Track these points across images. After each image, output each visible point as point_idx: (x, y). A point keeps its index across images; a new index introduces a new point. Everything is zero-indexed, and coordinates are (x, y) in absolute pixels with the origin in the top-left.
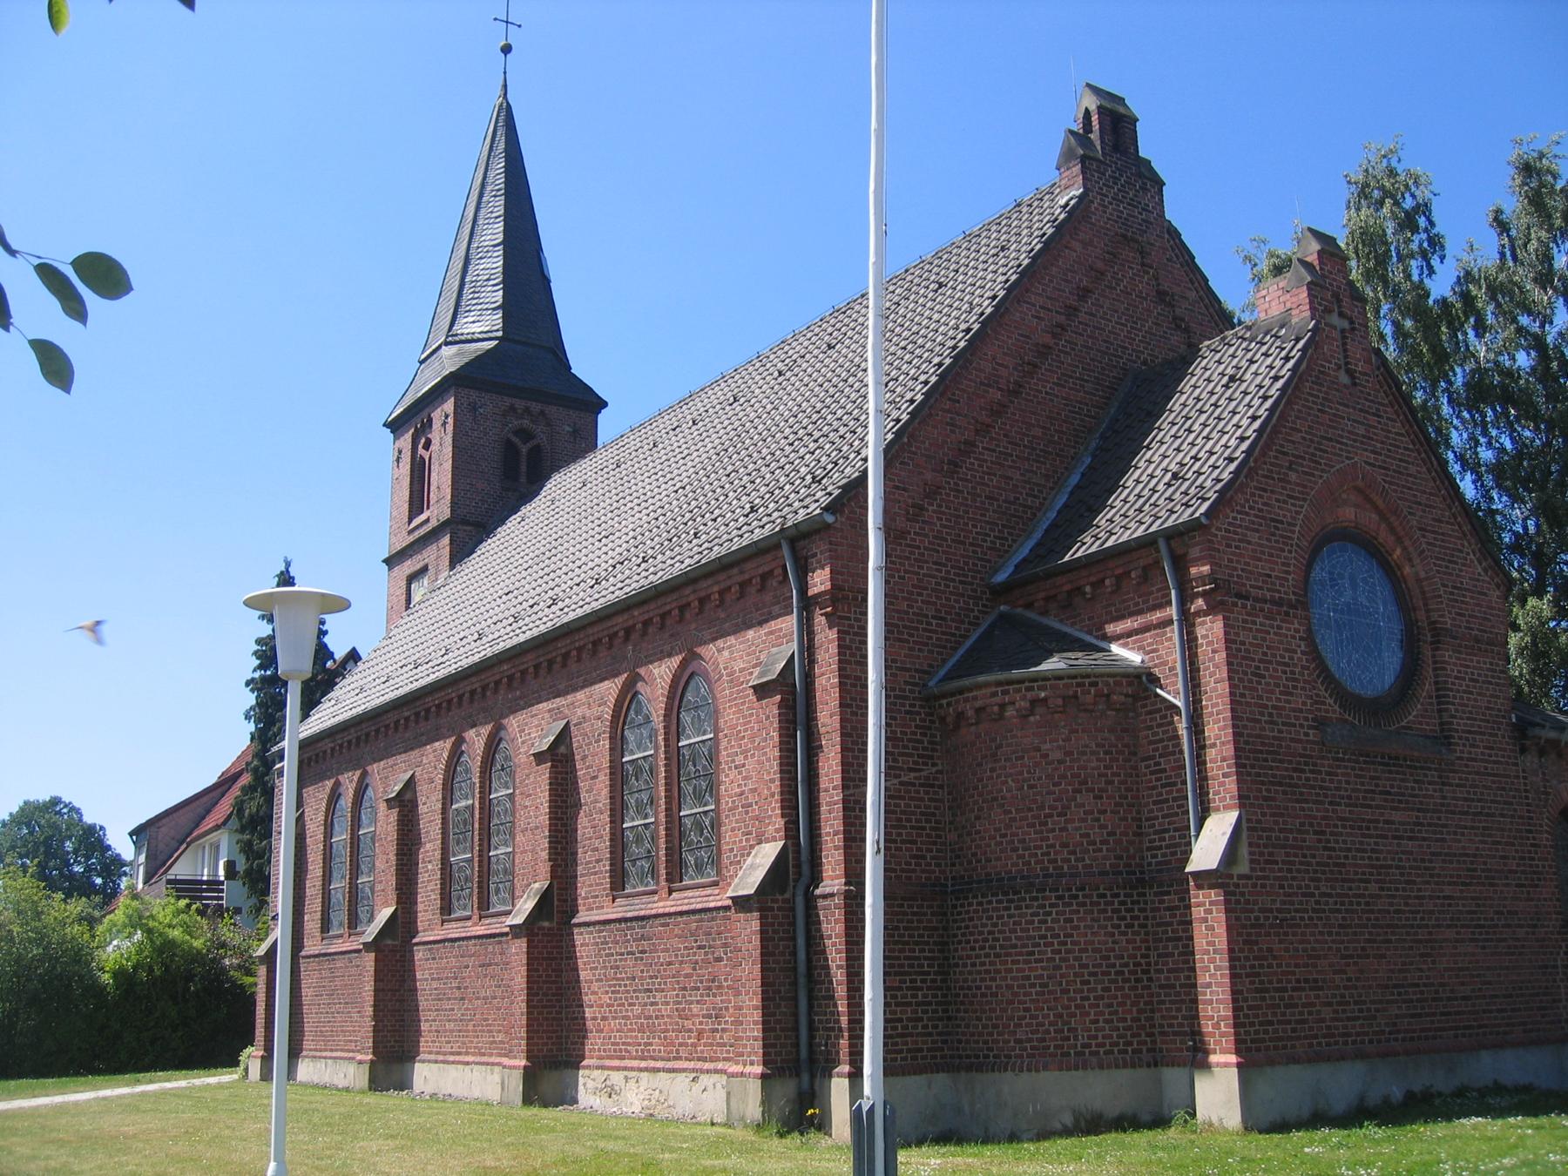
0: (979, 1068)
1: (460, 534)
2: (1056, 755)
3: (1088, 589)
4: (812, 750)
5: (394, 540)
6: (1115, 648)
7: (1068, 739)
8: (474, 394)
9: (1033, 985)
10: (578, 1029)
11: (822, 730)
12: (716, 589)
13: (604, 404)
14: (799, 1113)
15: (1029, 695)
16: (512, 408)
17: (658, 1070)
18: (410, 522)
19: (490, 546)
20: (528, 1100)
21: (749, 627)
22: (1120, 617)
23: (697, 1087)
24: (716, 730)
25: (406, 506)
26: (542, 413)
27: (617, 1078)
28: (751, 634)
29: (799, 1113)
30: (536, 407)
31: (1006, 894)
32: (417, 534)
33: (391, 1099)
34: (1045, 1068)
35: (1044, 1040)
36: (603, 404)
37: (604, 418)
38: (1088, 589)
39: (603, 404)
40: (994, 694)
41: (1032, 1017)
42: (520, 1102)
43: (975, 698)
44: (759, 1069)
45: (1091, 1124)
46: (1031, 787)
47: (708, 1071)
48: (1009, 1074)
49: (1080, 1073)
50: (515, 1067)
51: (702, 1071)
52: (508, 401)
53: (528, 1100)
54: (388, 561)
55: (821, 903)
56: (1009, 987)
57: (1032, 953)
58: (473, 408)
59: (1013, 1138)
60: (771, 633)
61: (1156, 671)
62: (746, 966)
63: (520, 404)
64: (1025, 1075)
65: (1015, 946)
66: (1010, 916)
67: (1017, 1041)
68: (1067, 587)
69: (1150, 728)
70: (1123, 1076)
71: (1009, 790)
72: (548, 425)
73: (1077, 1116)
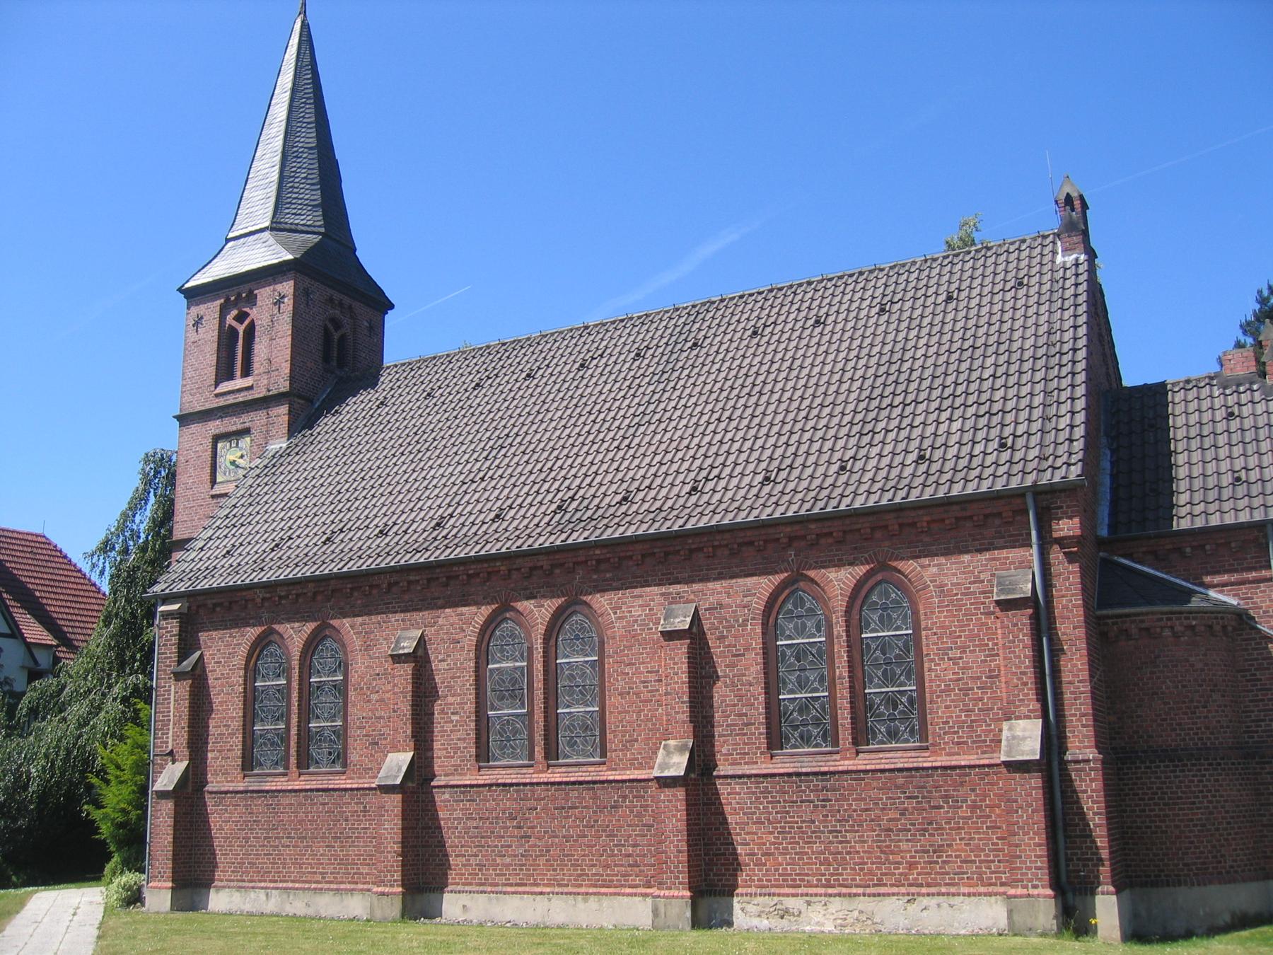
0: (1155, 884)
1: (296, 406)
2: (1200, 665)
3: (1188, 550)
4: (1056, 651)
5: (188, 398)
6: (1212, 593)
7: (1205, 655)
8: (307, 280)
9: (1195, 825)
10: (733, 865)
11: (1063, 638)
12: (925, 518)
13: (391, 306)
14: (1074, 920)
15: (1186, 622)
16: (331, 300)
17: (856, 895)
18: (216, 385)
19: (327, 422)
20: (696, 923)
21: (967, 552)
22: (1218, 572)
23: (911, 907)
24: (917, 628)
25: (213, 370)
26: (350, 307)
27: (791, 903)
28: (966, 557)
29: (1074, 920)
30: (347, 301)
31: (1171, 761)
32: (222, 402)
33: (423, 926)
34: (1211, 882)
35: (1204, 863)
36: (391, 306)
37: (390, 319)
38: (1188, 550)
39: (391, 306)
40: (1161, 619)
41: (1196, 848)
42: (688, 927)
43: (1142, 621)
44: (170, 884)
45: (1242, 922)
46: (1184, 686)
47: (923, 895)
48: (1183, 888)
49: (1232, 886)
50: (395, 894)
51: (919, 894)
52: (330, 291)
53: (696, 923)
54: (179, 418)
55: (1071, 766)
56: (1177, 827)
57: (1194, 803)
58: (307, 293)
59: (1188, 935)
60: (994, 559)
61: (1251, 612)
62: (1022, 816)
63: (337, 296)
64: (1196, 889)
65: (1181, 798)
66: (1176, 777)
67: (1185, 865)
68: (1170, 547)
69: (1246, 650)
70: (1254, 886)
71: (1168, 688)
72: (351, 317)
73: (1233, 915)
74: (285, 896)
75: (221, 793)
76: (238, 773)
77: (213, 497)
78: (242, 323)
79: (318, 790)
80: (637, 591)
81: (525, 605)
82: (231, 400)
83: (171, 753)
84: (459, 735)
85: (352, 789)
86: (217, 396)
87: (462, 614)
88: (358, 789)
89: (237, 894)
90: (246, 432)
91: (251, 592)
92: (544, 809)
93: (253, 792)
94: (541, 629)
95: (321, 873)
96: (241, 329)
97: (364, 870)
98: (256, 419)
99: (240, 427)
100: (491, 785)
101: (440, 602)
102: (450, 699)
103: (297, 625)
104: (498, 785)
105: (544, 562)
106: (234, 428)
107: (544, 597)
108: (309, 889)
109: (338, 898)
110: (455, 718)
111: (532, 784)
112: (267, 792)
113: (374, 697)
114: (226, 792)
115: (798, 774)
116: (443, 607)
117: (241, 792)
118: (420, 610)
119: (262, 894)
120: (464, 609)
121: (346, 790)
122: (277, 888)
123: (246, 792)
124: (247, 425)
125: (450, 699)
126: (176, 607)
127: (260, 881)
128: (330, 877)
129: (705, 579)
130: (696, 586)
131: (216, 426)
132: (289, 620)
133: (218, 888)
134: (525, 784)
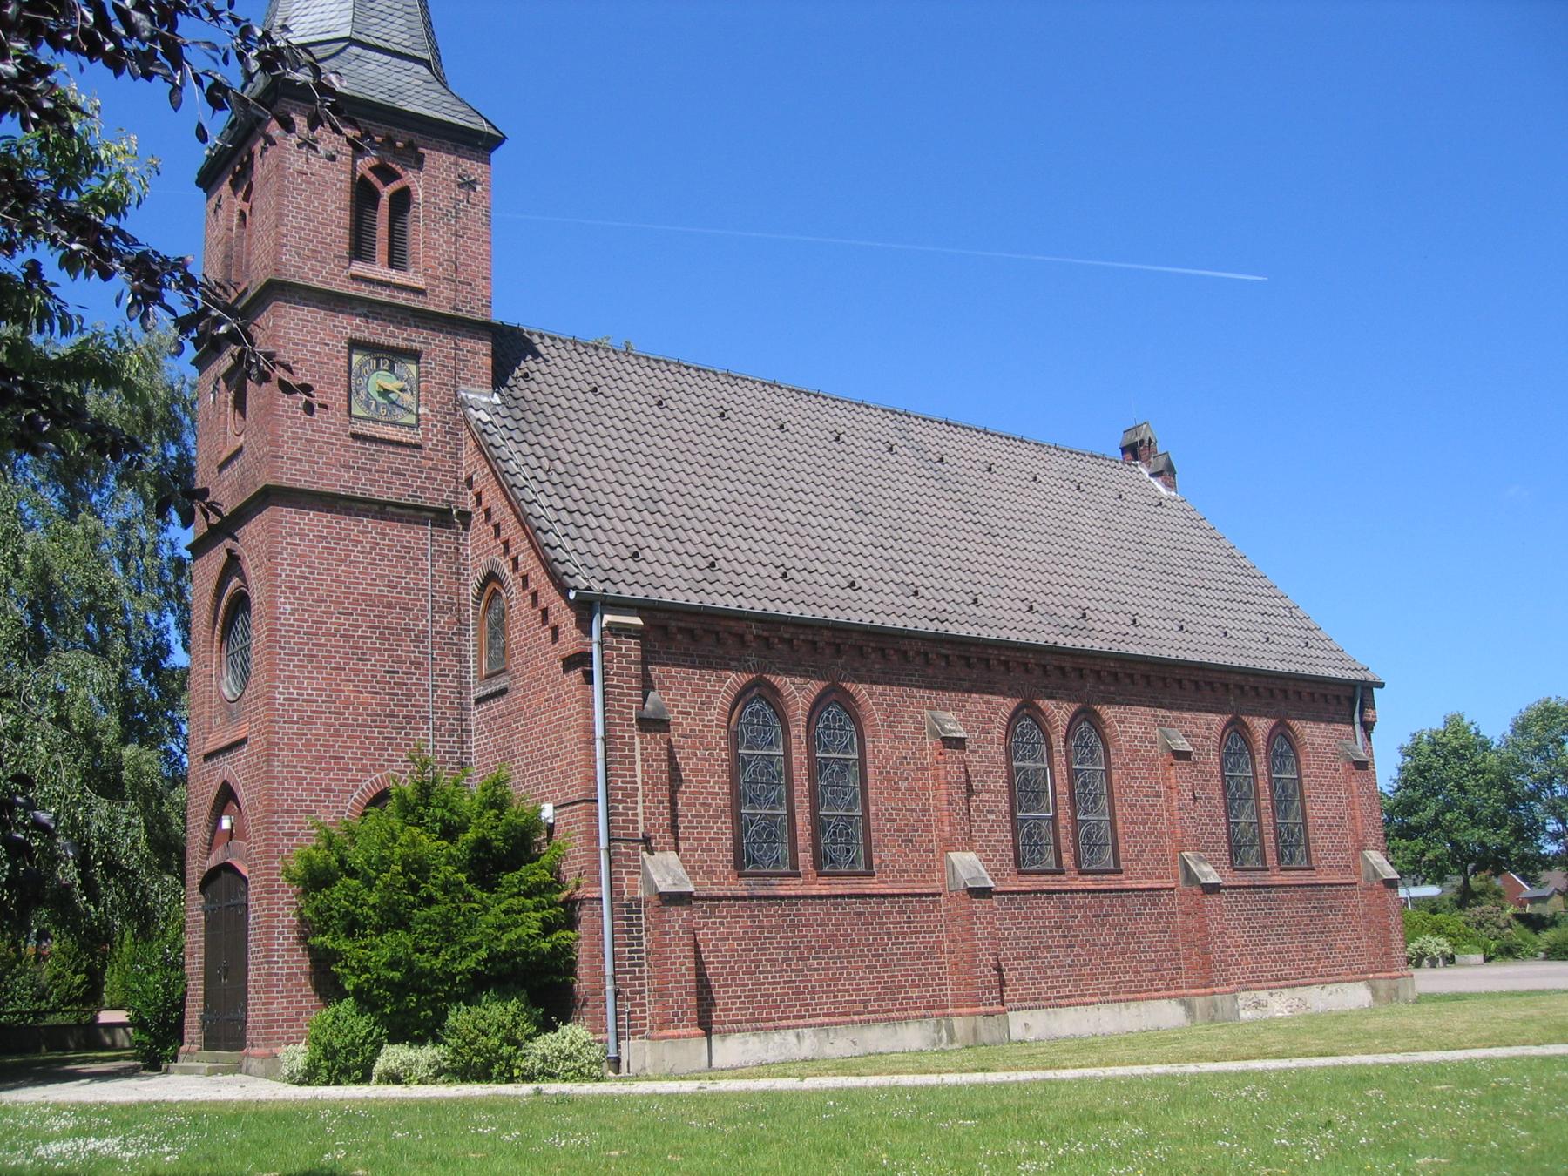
23: (1324, 993)
24: (1299, 773)
74: (823, 1035)
75: (712, 899)
76: (725, 870)
77: (355, 436)
78: (386, 184)
79: (850, 896)
80: (1135, 709)
81: (1046, 704)
82: (365, 291)
83: (646, 840)
84: (996, 836)
85: (893, 895)
86: (354, 278)
87: (989, 702)
88: (899, 895)
89: (755, 1039)
90: (415, 356)
91: (743, 624)
92: (1085, 916)
93: (760, 898)
94: (1062, 731)
95: (862, 1001)
96: (386, 192)
97: (915, 993)
98: (437, 346)
99: (403, 344)
100: (1036, 892)
101: (966, 684)
102: (985, 796)
103: (798, 680)
104: (1042, 892)
105: (1068, 664)
106: (392, 342)
107: (1062, 699)
108: (853, 1022)
109: (890, 1029)
110: (991, 817)
111: (1072, 891)
112: (782, 898)
113: (903, 784)
114: (719, 899)
115: (1255, 887)
116: (970, 691)
117: (743, 898)
118: (945, 689)
119: (790, 1035)
120: (990, 698)
121: (885, 896)
122: (810, 1026)
123: (751, 898)
124: (416, 345)
125: (985, 796)
126: (637, 621)
127: (780, 1019)
128: (873, 1006)
129: (1180, 709)
130: (1175, 714)
131: (352, 326)
132: (788, 673)
133: (723, 1034)
134: (1066, 892)
